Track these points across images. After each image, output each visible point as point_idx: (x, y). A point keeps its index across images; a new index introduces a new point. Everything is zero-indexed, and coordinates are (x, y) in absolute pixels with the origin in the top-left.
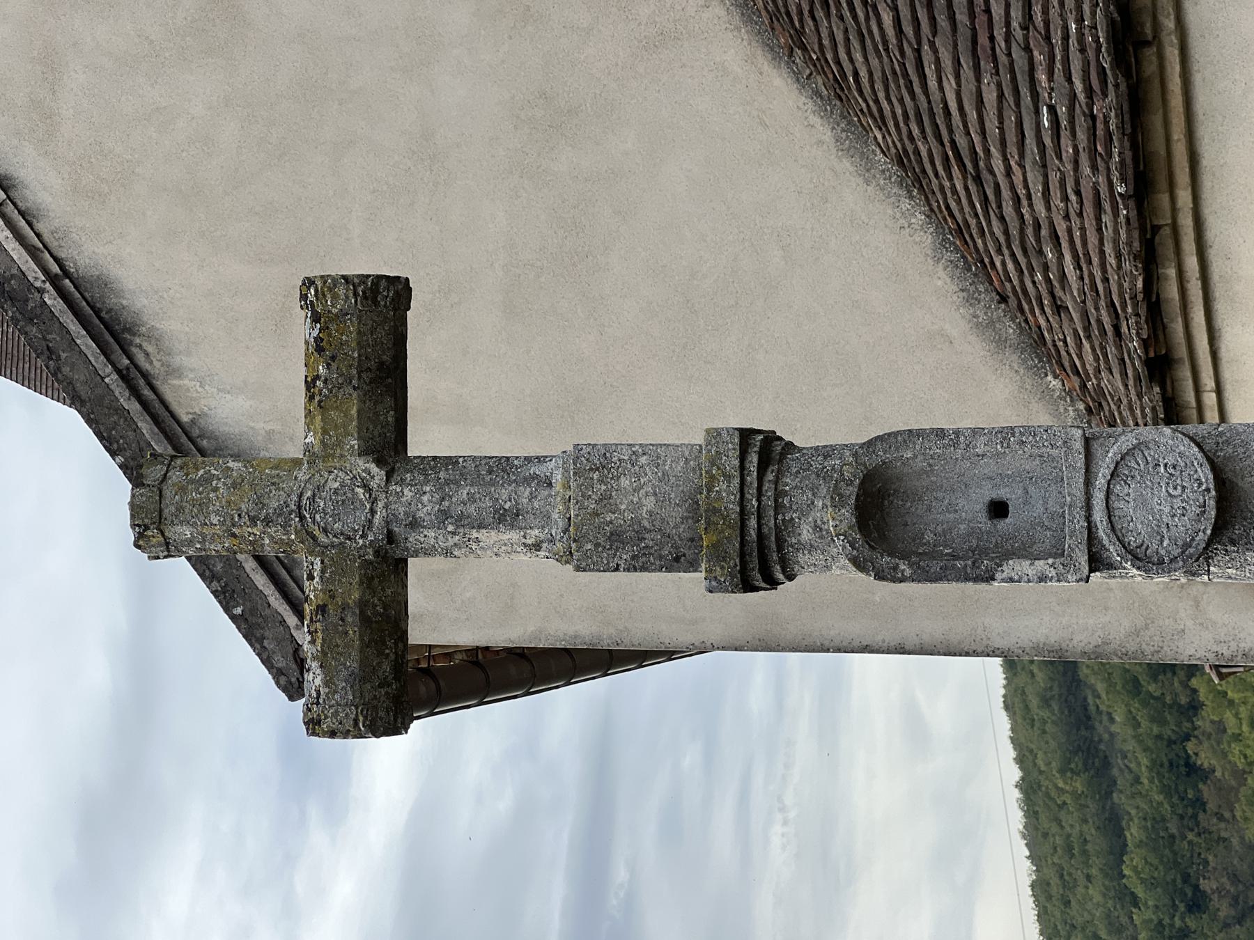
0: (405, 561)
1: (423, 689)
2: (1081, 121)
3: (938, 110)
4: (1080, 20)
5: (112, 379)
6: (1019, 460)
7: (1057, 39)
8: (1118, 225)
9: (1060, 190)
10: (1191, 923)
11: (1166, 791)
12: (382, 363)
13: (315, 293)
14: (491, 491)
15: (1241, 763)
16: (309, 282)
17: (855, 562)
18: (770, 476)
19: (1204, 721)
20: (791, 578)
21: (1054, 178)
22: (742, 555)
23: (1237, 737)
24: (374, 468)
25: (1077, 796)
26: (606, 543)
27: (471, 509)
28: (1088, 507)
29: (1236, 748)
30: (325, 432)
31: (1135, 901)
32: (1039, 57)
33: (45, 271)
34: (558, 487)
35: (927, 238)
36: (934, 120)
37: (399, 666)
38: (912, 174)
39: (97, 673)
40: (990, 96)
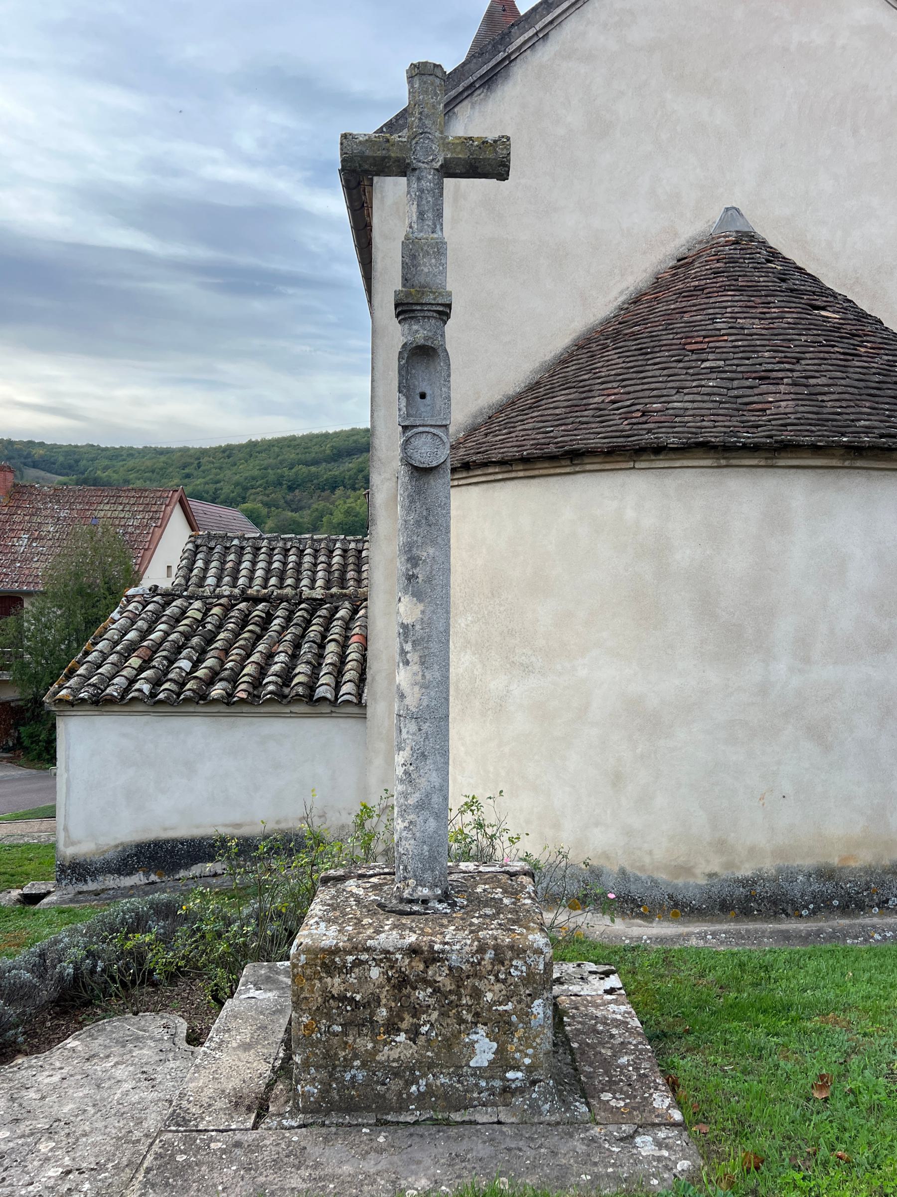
0: (405, 176)
1: (356, 204)
2: (548, 440)
3: (554, 394)
4: (581, 440)
5: (471, 80)
6: (439, 403)
7: (575, 432)
8: (513, 453)
9: (526, 435)
10: (285, 486)
11: (327, 480)
12: (477, 168)
13: (504, 142)
14: (431, 211)
15: (337, 503)
16: (508, 139)
17: (406, 344)
18: (435, 315)
19: (349, 492)
20: (400, 322)
21: (530, 432)
22: (408, 304)
23: (345, 502)
24: (440, 163)
25: (324, 451)
26: (412, 254)
27: (424, 202)
28: (423, 426)
29: (342, 502)
30: (453, 144)
31: (291, 469)
32: (569, 427)
33: (512, 53)
34: (432, 235)
35: (511, 392)
36: (551, 393)
37: (366, 172)
38: (534, 387)
39: (358, 86)
40: (557, 411)
